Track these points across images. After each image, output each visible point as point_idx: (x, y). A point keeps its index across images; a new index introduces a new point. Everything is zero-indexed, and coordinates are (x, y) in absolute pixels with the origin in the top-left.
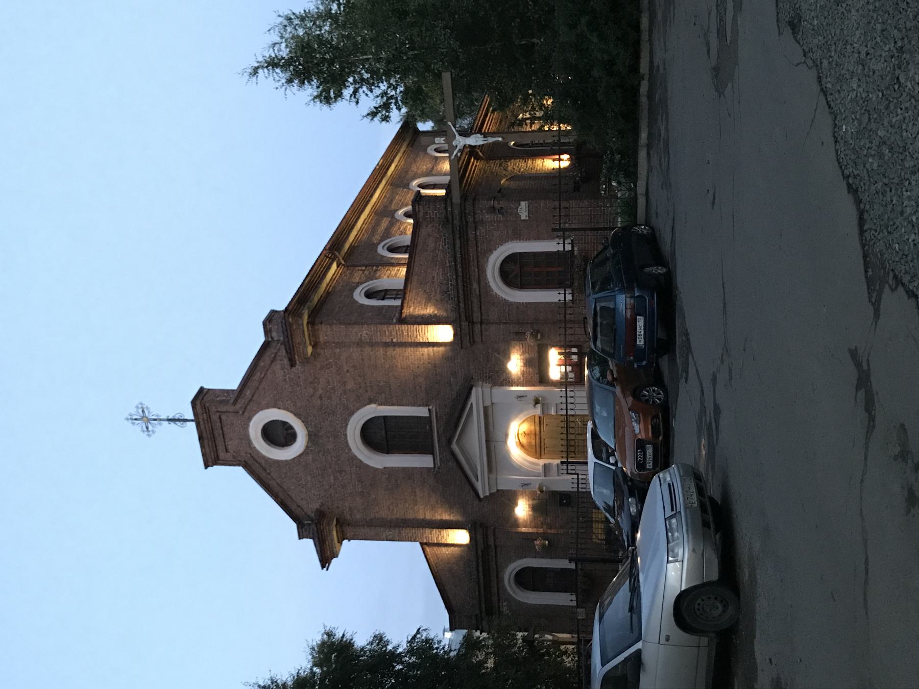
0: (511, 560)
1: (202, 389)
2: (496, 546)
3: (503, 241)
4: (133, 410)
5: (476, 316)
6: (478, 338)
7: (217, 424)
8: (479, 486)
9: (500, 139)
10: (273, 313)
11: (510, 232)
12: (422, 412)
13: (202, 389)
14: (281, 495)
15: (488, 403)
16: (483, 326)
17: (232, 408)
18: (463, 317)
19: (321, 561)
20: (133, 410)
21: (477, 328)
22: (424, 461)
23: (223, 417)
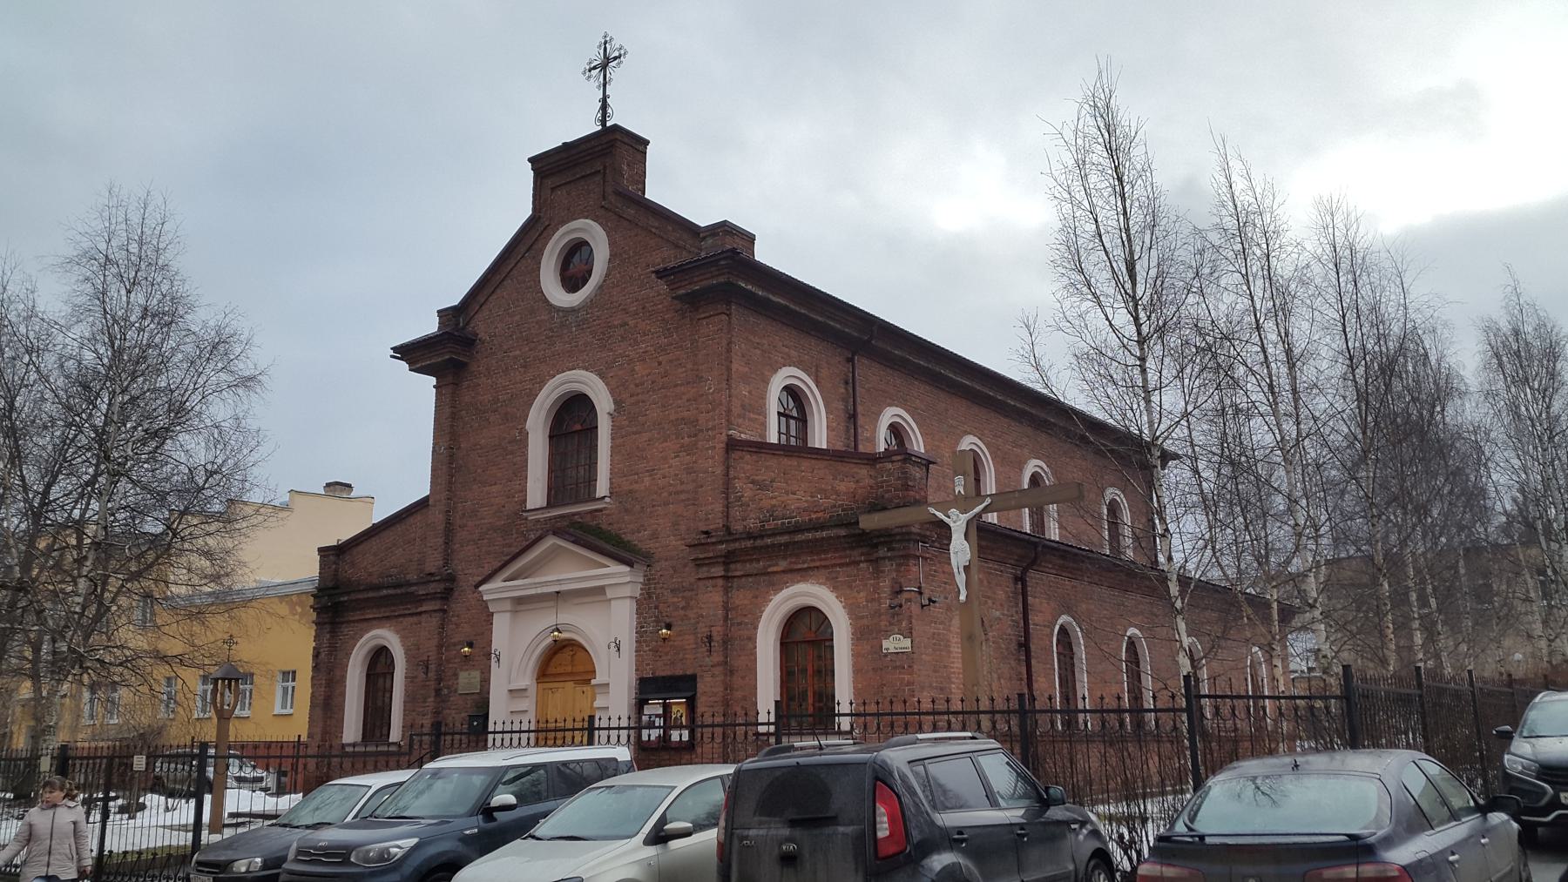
0: (404, 639)
1: (647, 142)
2: (420, 613)
3: (853, 611)
4: (616, 43)
5: (738, 569)
6: (704, 572)
7: (591, 173)
8: (496, 584)
9: (962, 597)
10: (751, 239)
11: (865, 621)
12: (602, 488)
13: (647, 142)
14: (498, 278)
15: (610, 594)
16: (720, 582)
17: (609, 190)
18: (733, 546)
19: (402, 346)
20: (616, 43)
21: (718, 571)
22: (536, 493)
23: (598, 178)
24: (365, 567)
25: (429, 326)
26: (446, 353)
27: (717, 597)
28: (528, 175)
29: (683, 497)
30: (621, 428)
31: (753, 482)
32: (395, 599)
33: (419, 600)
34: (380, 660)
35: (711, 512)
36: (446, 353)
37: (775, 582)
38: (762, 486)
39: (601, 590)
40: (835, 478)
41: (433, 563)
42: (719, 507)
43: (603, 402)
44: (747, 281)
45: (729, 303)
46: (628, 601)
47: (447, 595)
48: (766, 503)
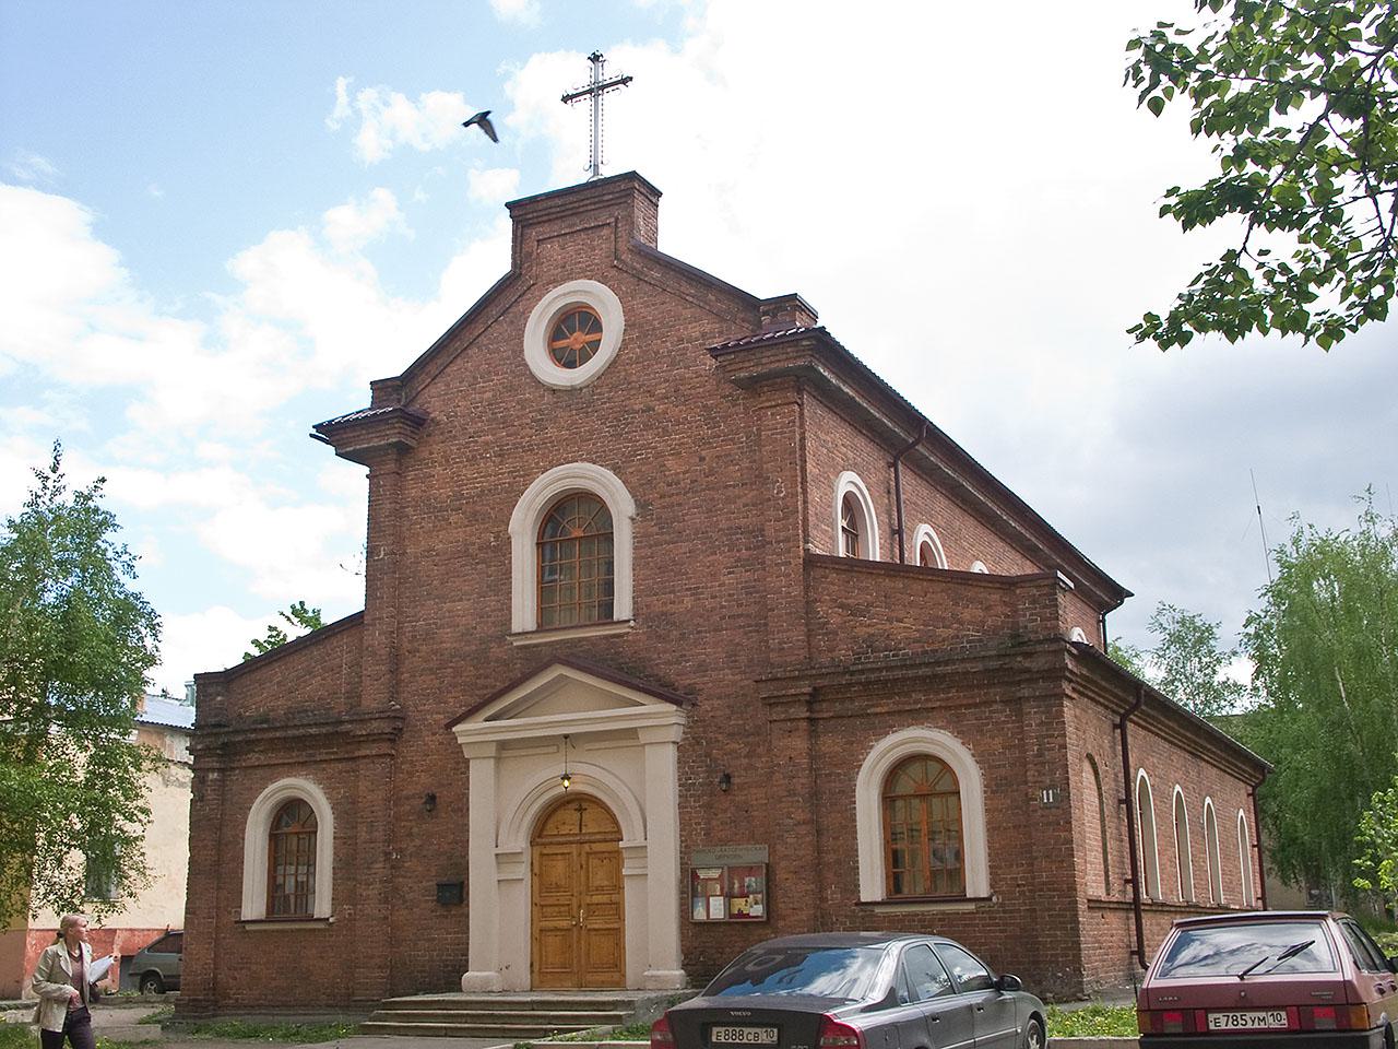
1: (659, 194)
3: (982, 758)
6: (778, 713)
11: (1003, 771)
13: (659, 194)
15: (643, 738)
17: (622, 246)
22: (524, 614)
24: (262, 700)
25: (359, 401)
26: (387, 433)
27: (799, 743)
28: (505, 224)
29: (741, 622)
30: (647, 535)
31: (842, 606)
32: (318, 740)
33: (360, 741)
34: (291, 819)
35: (789, 638)
36: (387, 433)
37: (273, 771)
38: (855, 612)
39: (632, 733)
40: (957, 604)
41: (373, 698)
42: (798, 635)
43: (621, 504)
44: (825, 366)
45: (800, 391)
46: (671, 746)
47: (394, 737)
48: (862, 632)
